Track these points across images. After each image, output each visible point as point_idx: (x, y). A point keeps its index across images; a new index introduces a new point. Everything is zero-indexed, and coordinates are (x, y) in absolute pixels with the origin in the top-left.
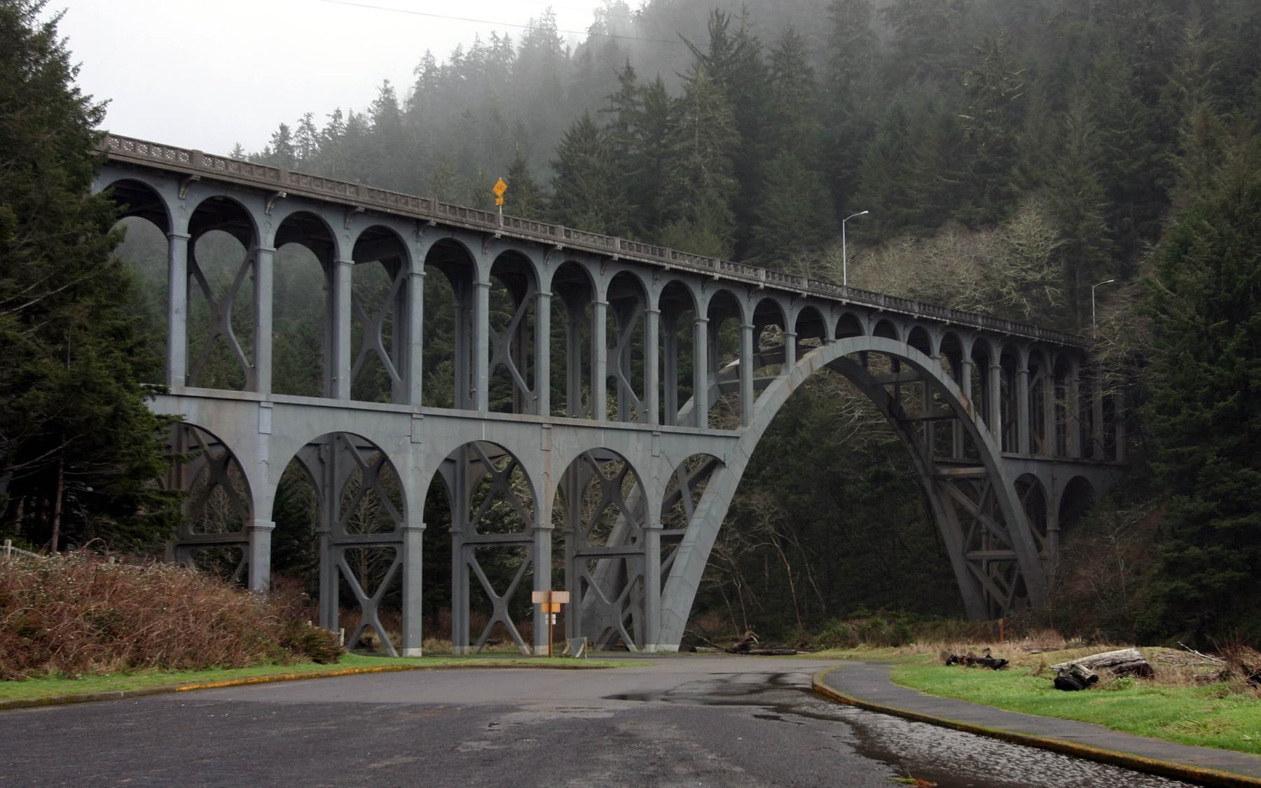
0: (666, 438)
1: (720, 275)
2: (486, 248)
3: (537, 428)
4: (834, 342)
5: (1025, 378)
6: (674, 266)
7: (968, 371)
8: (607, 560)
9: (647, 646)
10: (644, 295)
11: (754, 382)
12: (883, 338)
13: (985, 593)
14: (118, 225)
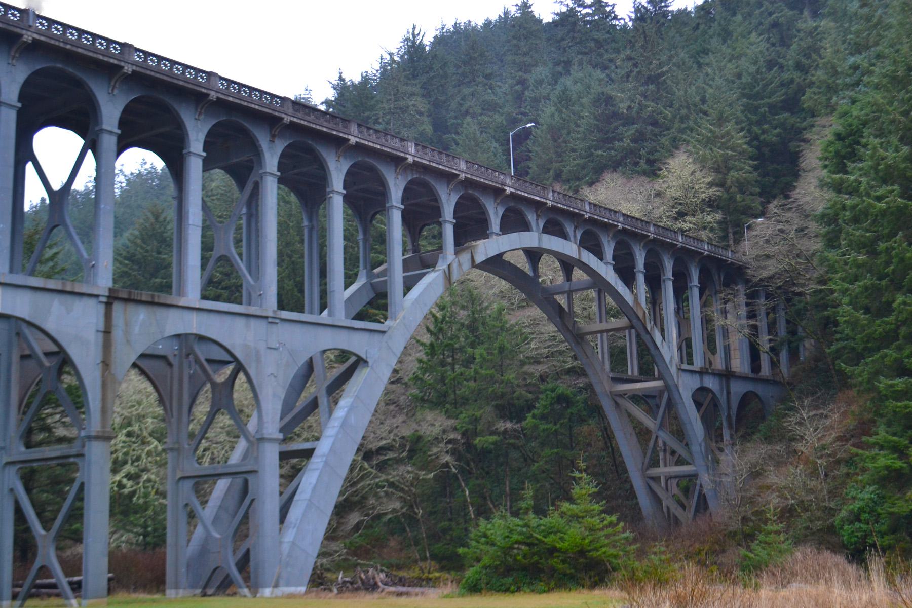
0: (287, 326)
1: (358, 140)
2: (498, 204)
4: (498, 235)
5: (696, 292)
6: (295, 120)
9: (261, 590)
10: (259, 154)
12: (553, 237)
13: (665, 509)
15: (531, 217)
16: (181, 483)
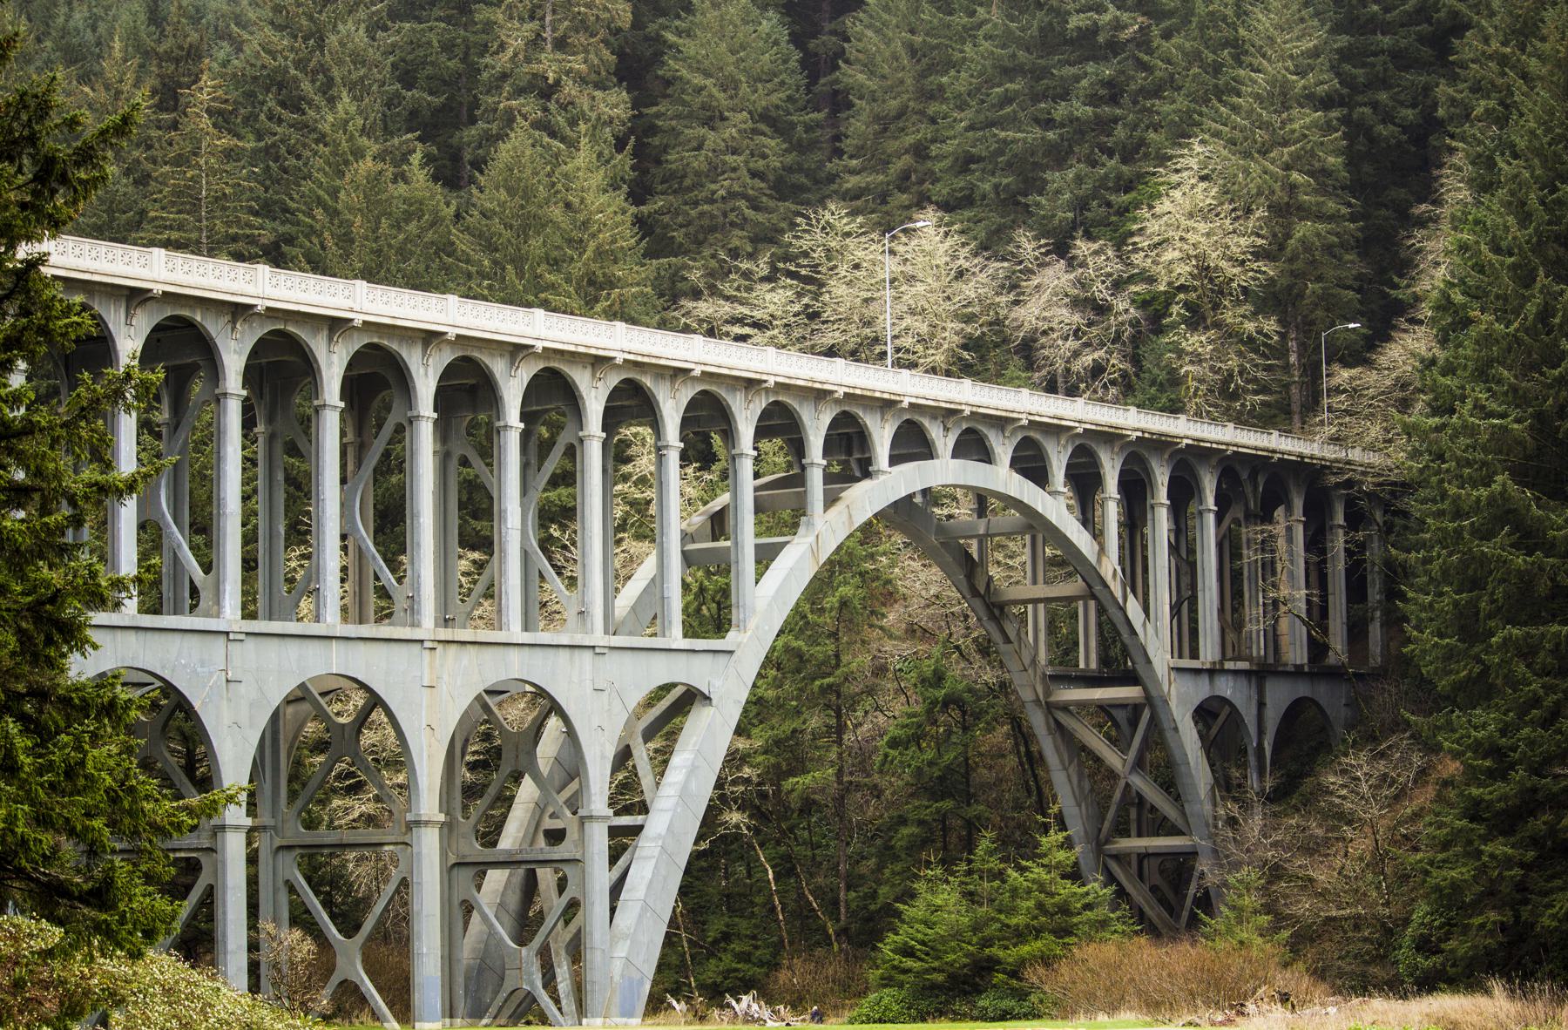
3: (416, 648)
7: (1112, 513)
8: (507, 872)
11: (757, 546)
14: (134, 414)
15: (935, 431)
16: (455, 871)
